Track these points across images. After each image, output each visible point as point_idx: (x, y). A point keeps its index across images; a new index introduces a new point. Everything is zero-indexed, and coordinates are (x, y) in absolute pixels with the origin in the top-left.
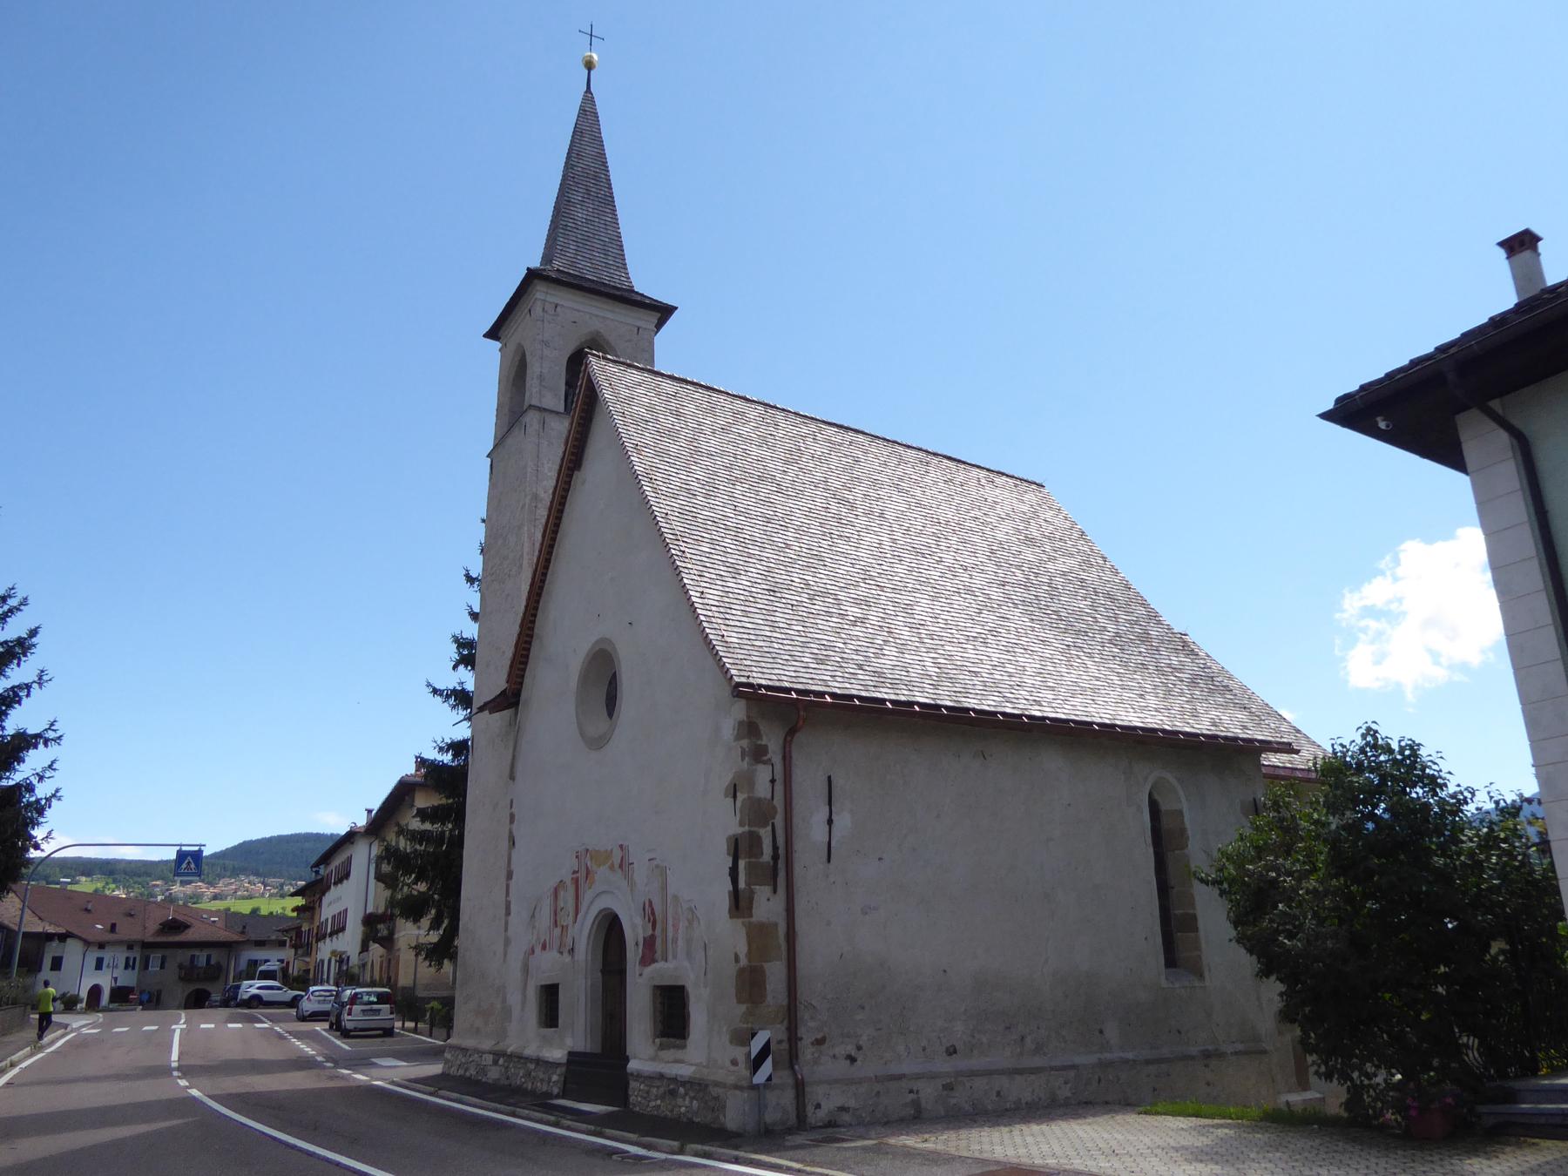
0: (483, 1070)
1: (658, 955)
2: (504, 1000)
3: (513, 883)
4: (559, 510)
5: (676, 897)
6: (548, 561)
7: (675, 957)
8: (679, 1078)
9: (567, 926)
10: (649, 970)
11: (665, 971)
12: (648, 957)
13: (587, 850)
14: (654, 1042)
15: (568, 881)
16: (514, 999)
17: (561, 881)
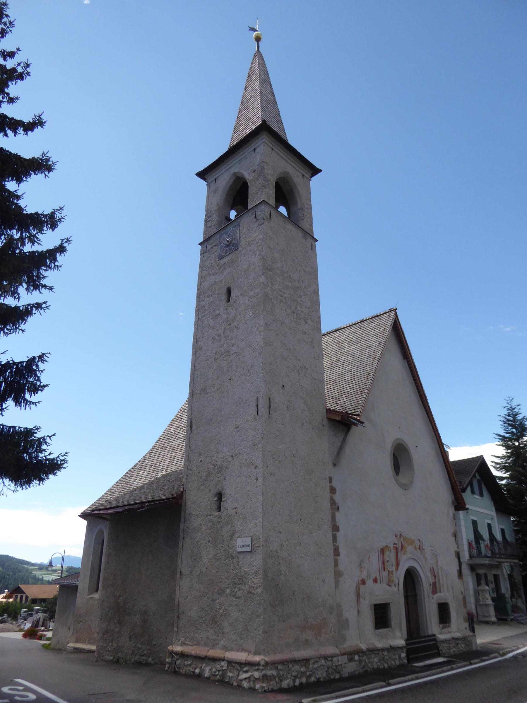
0: (337, 669)
1: (438, 590)
2: (340, 615)
3: (340, 535)
4: (409, 362)
5: (441, 568)
6: (415, 380)
7: (444, 591)
8: (459, 638)
9: (392, 572)
10: (435, 596)
11: (441, 596)
12: (434, 592)
13: (401, 535)
14: (440, 626)
15: (391, 546)
16: (350, 614)
17: (387, 546)
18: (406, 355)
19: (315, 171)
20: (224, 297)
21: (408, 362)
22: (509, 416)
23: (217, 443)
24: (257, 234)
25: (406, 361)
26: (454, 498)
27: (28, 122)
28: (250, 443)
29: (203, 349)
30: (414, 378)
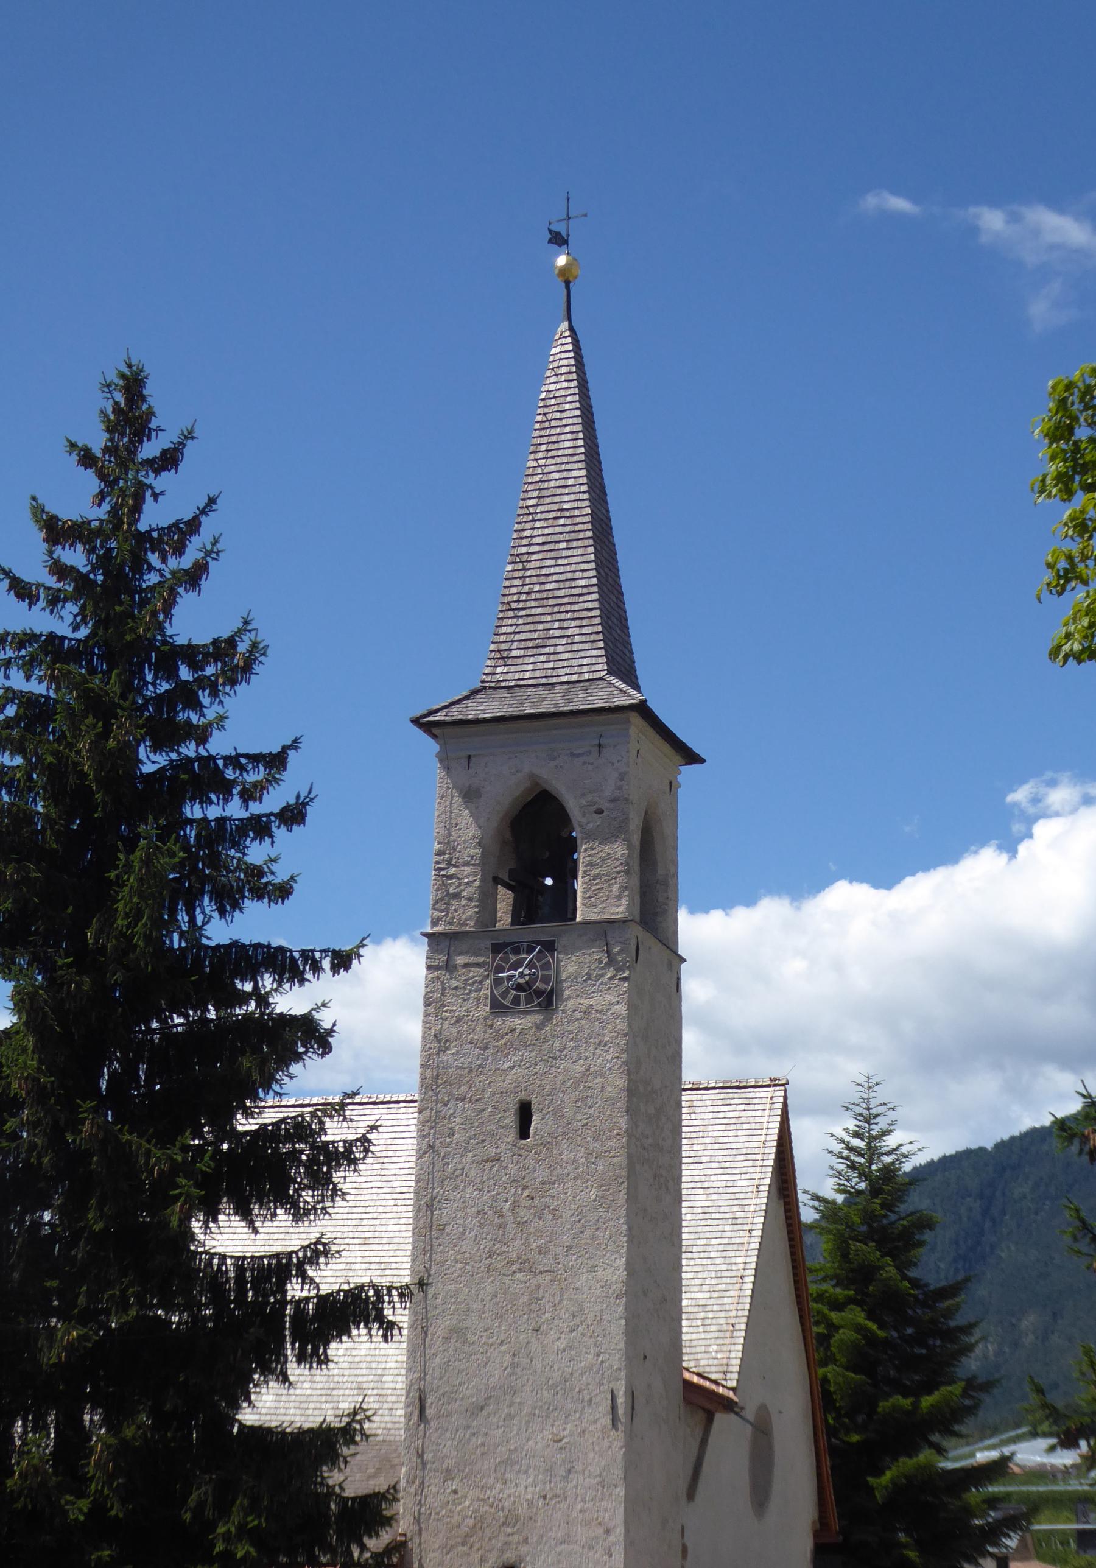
18: (786, 1189)
19: (692, 758)
20: (511, 1120)
21: (786, 1204)
22: (857, 1135)
23: (499, 1463)
24: (609, 998)
25: (782, 1202)
26: (817, 1518)
27: (295, 827)
28: (594, 1481)
29: (448, 1229)
30: (792, 1236)
